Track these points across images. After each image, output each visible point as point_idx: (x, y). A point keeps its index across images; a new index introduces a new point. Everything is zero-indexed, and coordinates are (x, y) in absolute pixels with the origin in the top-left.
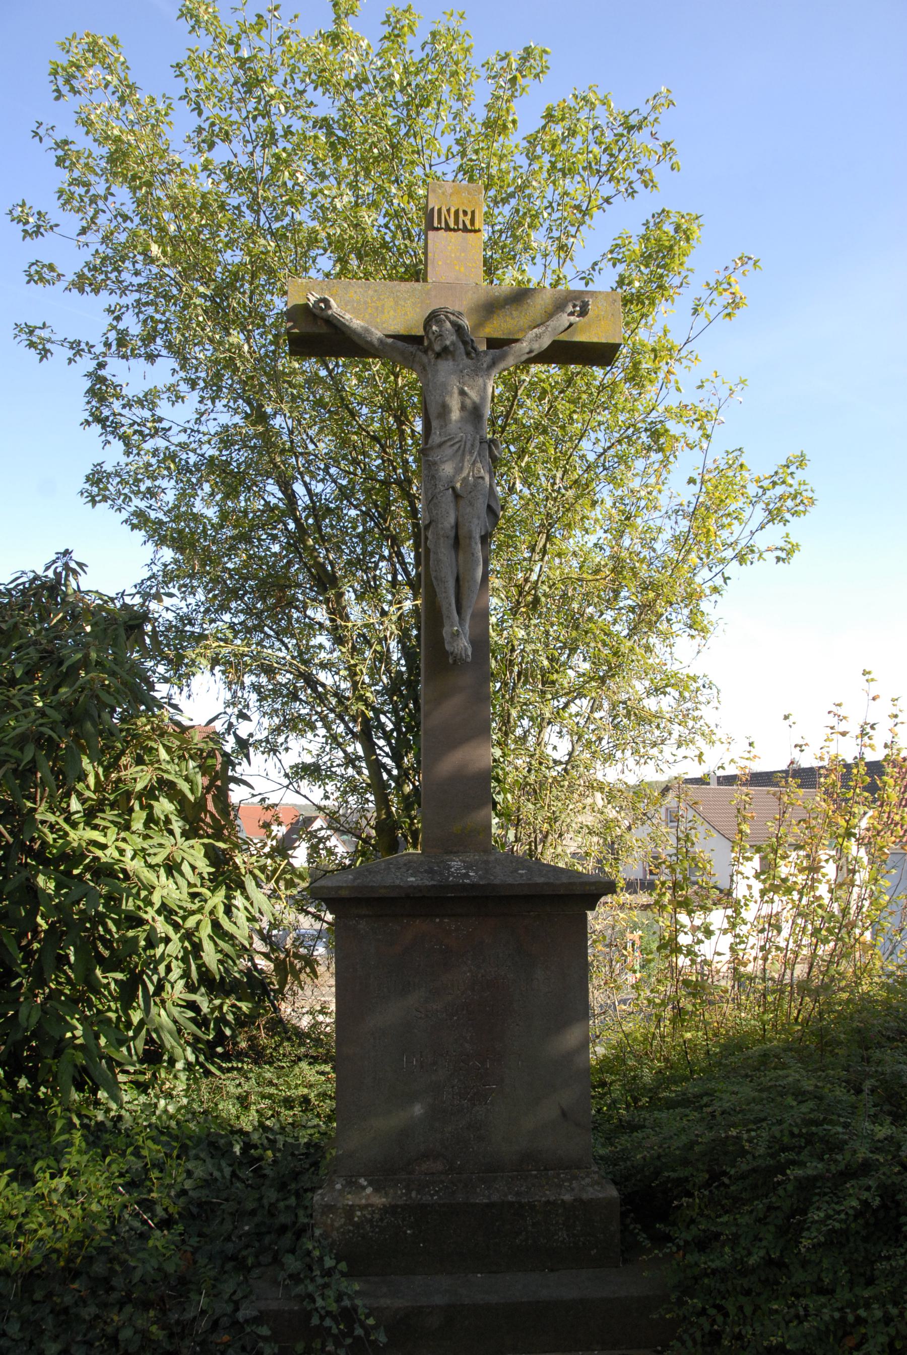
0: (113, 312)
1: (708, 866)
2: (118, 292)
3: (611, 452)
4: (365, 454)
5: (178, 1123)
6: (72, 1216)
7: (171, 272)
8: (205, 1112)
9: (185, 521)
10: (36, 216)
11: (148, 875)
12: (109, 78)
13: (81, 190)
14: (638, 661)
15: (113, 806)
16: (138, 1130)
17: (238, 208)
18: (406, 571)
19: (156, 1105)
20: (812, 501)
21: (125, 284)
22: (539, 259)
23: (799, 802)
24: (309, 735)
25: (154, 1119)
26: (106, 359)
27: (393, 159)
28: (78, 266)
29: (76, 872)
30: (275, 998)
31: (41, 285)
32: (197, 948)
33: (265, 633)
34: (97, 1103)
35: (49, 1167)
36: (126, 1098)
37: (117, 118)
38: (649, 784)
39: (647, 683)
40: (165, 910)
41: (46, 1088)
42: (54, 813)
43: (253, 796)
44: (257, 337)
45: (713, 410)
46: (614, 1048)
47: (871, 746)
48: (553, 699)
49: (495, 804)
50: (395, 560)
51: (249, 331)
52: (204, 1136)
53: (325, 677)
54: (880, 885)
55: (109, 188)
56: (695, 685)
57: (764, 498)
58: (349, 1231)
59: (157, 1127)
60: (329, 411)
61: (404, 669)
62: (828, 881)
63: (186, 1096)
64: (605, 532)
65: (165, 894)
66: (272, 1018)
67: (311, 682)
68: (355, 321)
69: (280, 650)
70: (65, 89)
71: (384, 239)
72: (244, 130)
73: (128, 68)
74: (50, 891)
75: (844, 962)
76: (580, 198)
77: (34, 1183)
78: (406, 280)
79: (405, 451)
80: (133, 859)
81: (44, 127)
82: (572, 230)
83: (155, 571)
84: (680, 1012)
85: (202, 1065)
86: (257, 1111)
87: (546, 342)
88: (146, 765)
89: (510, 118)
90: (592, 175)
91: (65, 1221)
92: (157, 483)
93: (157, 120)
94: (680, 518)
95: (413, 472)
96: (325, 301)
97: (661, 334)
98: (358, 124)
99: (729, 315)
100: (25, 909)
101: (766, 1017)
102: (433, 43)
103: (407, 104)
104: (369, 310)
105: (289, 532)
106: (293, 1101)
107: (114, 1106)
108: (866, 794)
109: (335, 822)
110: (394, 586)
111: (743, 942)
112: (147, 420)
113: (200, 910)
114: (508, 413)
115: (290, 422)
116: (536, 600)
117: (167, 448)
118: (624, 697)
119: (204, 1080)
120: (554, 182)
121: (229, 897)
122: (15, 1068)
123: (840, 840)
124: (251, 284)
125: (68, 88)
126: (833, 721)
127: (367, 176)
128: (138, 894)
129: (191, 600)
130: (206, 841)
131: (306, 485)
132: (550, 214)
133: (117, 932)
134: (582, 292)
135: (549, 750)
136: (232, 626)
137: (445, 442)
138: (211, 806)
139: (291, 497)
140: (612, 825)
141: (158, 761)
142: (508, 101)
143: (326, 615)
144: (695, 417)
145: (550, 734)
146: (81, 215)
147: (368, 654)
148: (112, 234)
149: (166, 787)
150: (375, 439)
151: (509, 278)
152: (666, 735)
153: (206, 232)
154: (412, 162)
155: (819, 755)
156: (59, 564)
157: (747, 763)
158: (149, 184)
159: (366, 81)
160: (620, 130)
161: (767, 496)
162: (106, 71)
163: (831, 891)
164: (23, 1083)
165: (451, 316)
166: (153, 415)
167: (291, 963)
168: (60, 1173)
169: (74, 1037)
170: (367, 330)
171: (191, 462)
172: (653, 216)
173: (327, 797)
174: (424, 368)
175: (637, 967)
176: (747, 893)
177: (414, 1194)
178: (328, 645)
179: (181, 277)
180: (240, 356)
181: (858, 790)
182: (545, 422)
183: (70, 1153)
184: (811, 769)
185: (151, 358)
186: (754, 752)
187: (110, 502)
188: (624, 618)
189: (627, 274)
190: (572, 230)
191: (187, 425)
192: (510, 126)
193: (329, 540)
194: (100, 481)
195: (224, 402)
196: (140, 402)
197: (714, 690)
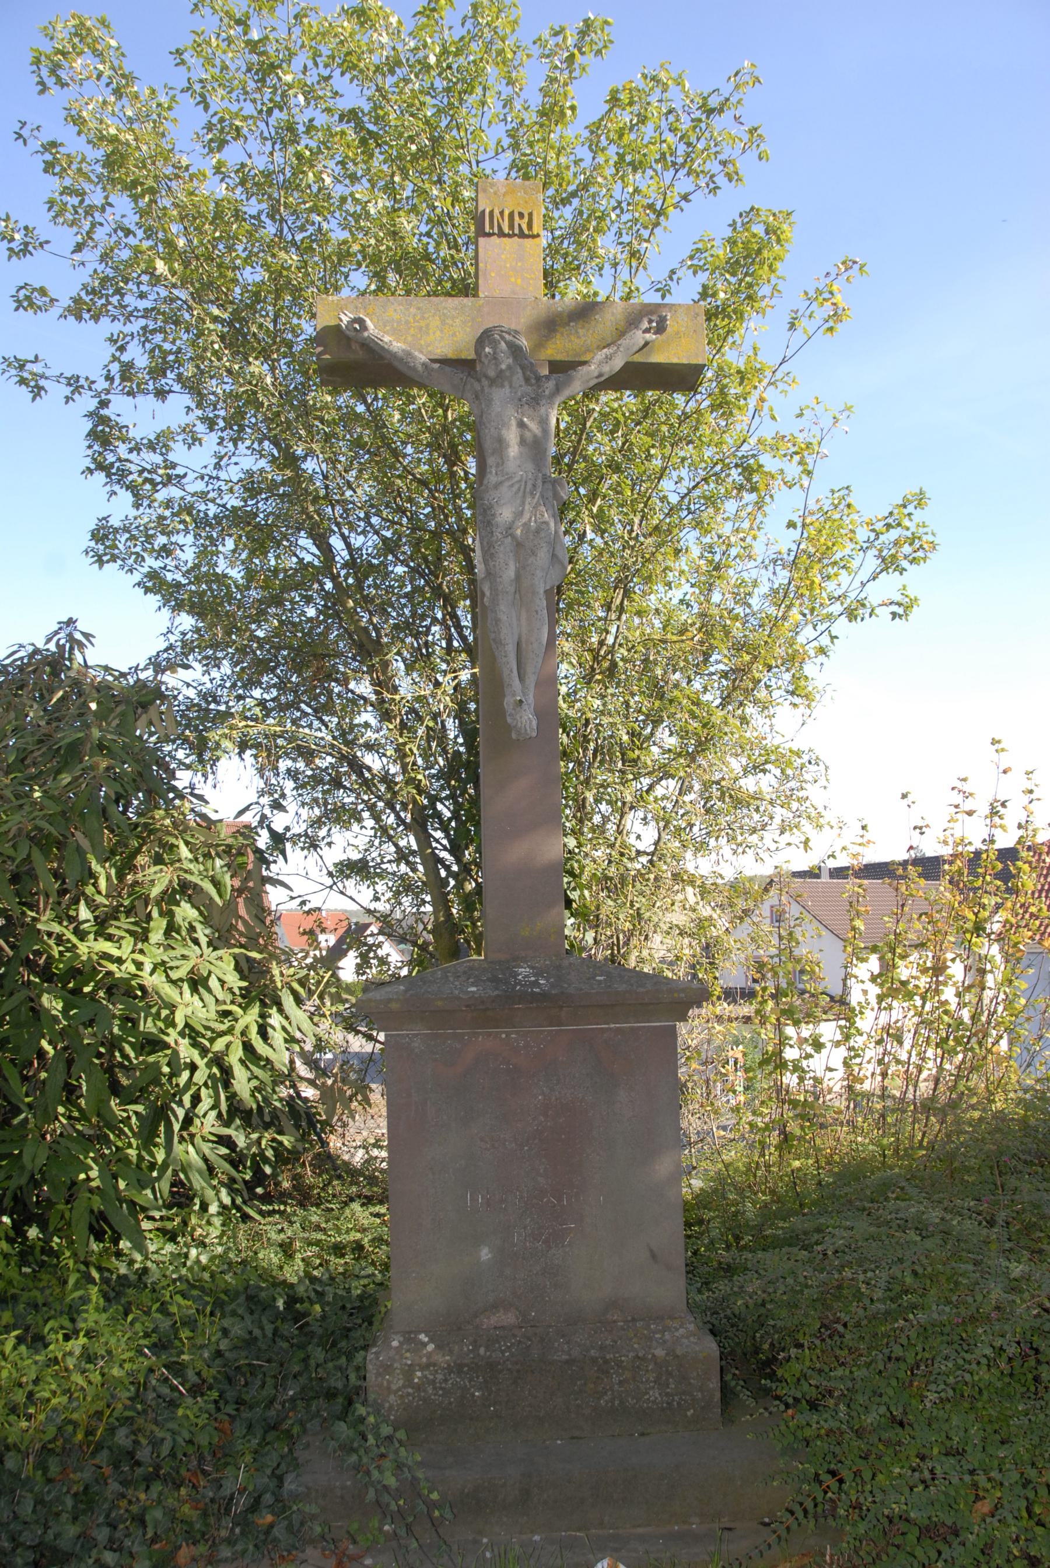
0: (116, 342)
1: (817, 969)
2: (122, 318)
3: (697, 493)
4: (410, 500)
5: (212, 1276)
6: (90, 1383)
7: (182, 294)
8: (244, 1262)
9: (206, 583)
10: (23, 232)
11: (169, 991)
12: (101, 67)
13: (75, 201)
14: (732, 733)
15: (128, 913)
16: (164, 1283)
17: (257, 217)
18: (464, 638)
19: (186, 1256)
20: (934, 546)
21: (129, 309)
22: (608, 270)
23: (921, 893)
24: (355, 827)
25: (184, 1271)
26: (109, 397)
27: (434, 156)
28: (75, 290)
29: (87, 989)
30: (323, 1130)
31: (31, 311)
32: (227, 1073)
33: (303, 711)
34: (119, 1254)
35: (62, 1328)
36: (152, 1248)
37: (113, 114)
38: (751, 879)
39: (744, 761)
40: (190, 1032)
41: (60, 1238)
42: (60, 923)
43: (292, 898)
44: (284, 367)
45: (815, 442)
46: (712, 1179)
47: (1002, 826)
48: (635, 779)
49: (568, 902)
50: (450, 623)
51: (273, 361)
52: (241, 1289)
53: (372, 761)
54: (1015, 987)
55: (106, 198)
56: (799, 761)
57: (876, 543)
58: (409, 1394)
59: (187, 1281)
60: (369, 452)
61: (462, 749)
62: (955, 984)
63: (221, 1245)
64: (692, 586)
65: (189, 1013)
66: (319, 1154)
67: (357, 767)
68: (394, 344)
69: (320, 729)
70: (50, 81)
71: (426, 250)
72: (262, 126)
73: (123, 55)
74: (54, 1012)
75: (974, 1077)
76: (653, 196)
77: (46, 1346)
78: (451, 295)
79: (458, 496)
80: (152, 973)
81: (28, 127)
82: (645, 234)
83: (172, 641)
84: (786, 1137)
85: (239, 1209)
86: (303, 1260)
87: (618, 363)
88: (166, 865)
89: (568, 104)
90: (665, 168)
91: (82, 1389)
92: (173, 539)
93: (159, 116)
94: (778, 568)
95: (467, 520)
96: (361, 321)
97: (751, 353)
98: (392, 116)
99: (831, 329)
100: (28, 1032)
101: (885, 1141)
102: (474, 17)
103: (448, 90)
104: (412, 331)
105: (327, 593)
106: (344, 1247)
107: (138, 1257)
108: (999, 883)
109: (388, 926)
110: (449, 654)
111: (859, 1056)
112: (158, 466)
113: (230, 1031)
114: (576, 448)
115: (324, 466)
116: (614, 665)
117: (182, 498)
118: (717, 776)
119: (242, 1226)
120: (622, 178)
121: (263, 1016)
122: (23, 1218)
123: (968, 936)
124: (275, 305)
125: (54, 79)
126: (958, 799)
127: (405, 176)
128: (158, 1014)
129: (215, 673)
130: (237, 951)
131: (345, 539)
132: (618, 216)
133: (137, 1058)
134: (659, 305)
135: (632, 840)
136: (262, 703)
137: (501, 483)
138: (242, 911)
139: (327, 551)
140: (706, 924)
141: (179, 860)
142: (566, 84)
143: (370, 689)
144: (794, 449)
145: (633, 821)
146: (75, 229)
147: (421, 732)
148: (112, 250)
149: (185, 889)
150: (423, 483)
151: (573, 291)
152: (766, 819)
153: (221, 247)
154: (458, 159)
155: (942, 839)
156: (62, 635)
157: (860, 849)
158: (152, 191)
159: (398, 63)
160: (698, 114)
161: (880, 541)
162: (97, 59)
163: (958, 995)
164: (33, 1232)
165: (507, 336)
166: (165, 461)
167: (340, 1090)
168: (76, 1332)
169: (89, 1179)
170: (409, 354)
171: (211, 514)
172: (741, 215)
173: (376, 899)
174: (477, 397)
175: (740, 1089)
176: (862, 1000)
177: (482, 1351)
178: (373, 722)
179: (194, 299)
180: (263, 389)
181: (988, 878)
182: (619, 458)
183: (86, 1311)
184: (937, 858)
185: (161, 394)
186: (868, 836)
187: (119, 562)
188: (716, 685)
189: (711, 284)
190: (645, 234)
191: (204, 471)
192: (569, 113)
193: (372, 600)
194: (106, 537)
195: (248, 443)
196: (152, 447)
197: (822, 767)
